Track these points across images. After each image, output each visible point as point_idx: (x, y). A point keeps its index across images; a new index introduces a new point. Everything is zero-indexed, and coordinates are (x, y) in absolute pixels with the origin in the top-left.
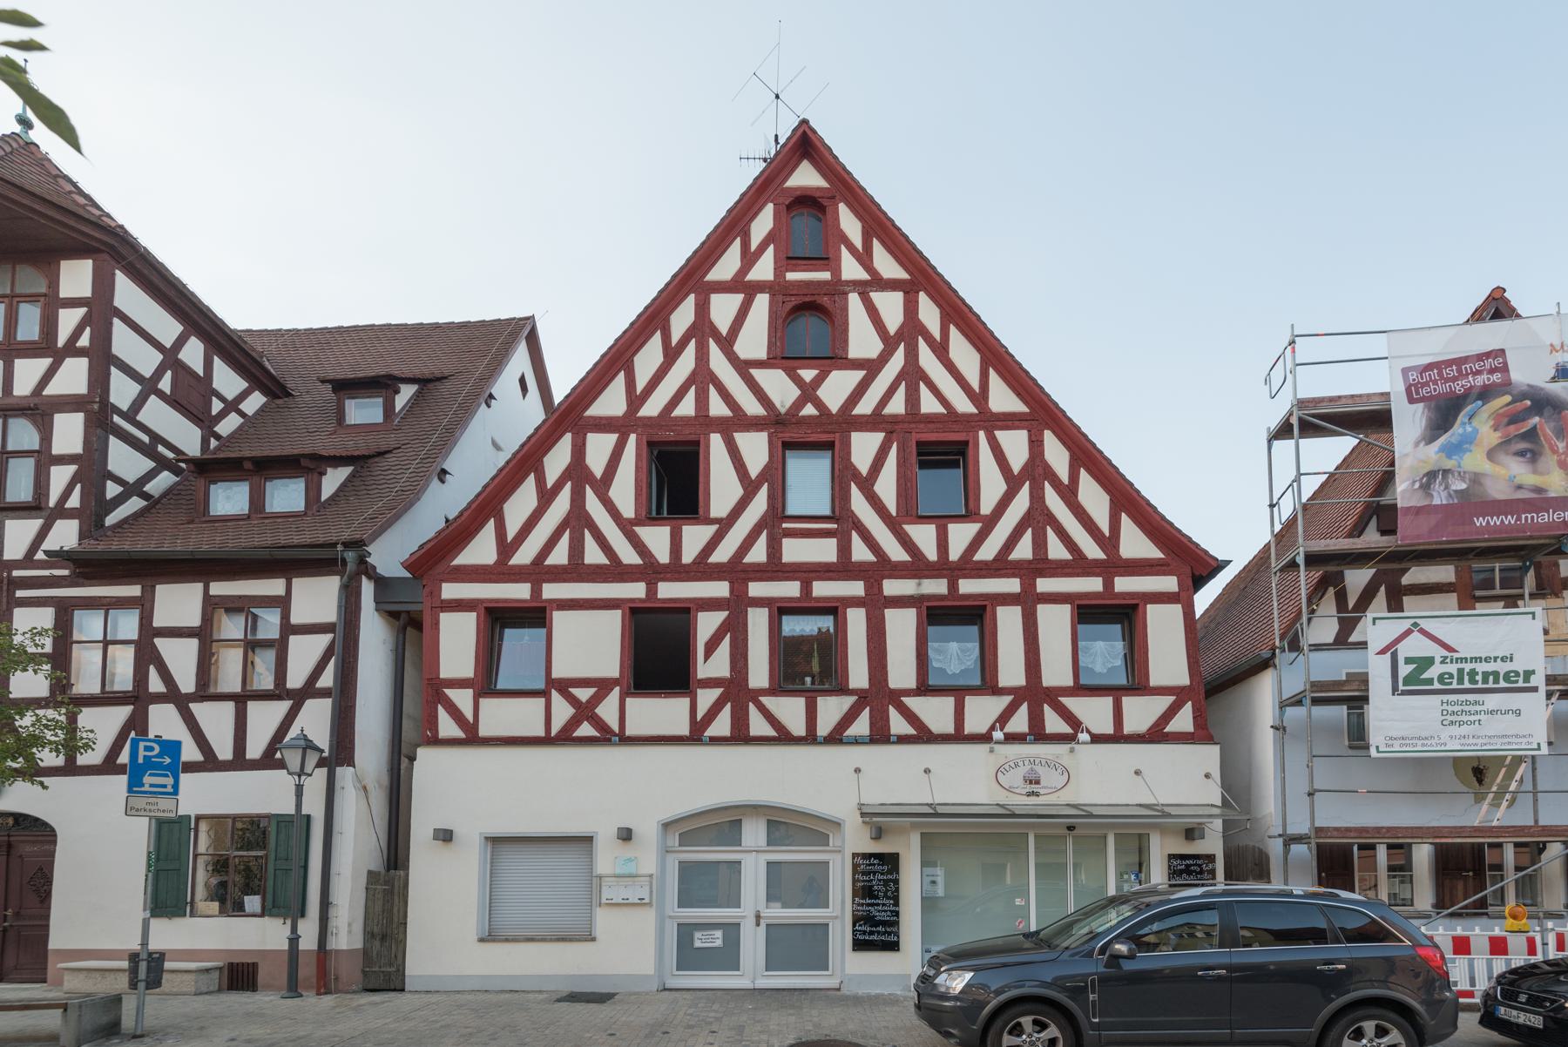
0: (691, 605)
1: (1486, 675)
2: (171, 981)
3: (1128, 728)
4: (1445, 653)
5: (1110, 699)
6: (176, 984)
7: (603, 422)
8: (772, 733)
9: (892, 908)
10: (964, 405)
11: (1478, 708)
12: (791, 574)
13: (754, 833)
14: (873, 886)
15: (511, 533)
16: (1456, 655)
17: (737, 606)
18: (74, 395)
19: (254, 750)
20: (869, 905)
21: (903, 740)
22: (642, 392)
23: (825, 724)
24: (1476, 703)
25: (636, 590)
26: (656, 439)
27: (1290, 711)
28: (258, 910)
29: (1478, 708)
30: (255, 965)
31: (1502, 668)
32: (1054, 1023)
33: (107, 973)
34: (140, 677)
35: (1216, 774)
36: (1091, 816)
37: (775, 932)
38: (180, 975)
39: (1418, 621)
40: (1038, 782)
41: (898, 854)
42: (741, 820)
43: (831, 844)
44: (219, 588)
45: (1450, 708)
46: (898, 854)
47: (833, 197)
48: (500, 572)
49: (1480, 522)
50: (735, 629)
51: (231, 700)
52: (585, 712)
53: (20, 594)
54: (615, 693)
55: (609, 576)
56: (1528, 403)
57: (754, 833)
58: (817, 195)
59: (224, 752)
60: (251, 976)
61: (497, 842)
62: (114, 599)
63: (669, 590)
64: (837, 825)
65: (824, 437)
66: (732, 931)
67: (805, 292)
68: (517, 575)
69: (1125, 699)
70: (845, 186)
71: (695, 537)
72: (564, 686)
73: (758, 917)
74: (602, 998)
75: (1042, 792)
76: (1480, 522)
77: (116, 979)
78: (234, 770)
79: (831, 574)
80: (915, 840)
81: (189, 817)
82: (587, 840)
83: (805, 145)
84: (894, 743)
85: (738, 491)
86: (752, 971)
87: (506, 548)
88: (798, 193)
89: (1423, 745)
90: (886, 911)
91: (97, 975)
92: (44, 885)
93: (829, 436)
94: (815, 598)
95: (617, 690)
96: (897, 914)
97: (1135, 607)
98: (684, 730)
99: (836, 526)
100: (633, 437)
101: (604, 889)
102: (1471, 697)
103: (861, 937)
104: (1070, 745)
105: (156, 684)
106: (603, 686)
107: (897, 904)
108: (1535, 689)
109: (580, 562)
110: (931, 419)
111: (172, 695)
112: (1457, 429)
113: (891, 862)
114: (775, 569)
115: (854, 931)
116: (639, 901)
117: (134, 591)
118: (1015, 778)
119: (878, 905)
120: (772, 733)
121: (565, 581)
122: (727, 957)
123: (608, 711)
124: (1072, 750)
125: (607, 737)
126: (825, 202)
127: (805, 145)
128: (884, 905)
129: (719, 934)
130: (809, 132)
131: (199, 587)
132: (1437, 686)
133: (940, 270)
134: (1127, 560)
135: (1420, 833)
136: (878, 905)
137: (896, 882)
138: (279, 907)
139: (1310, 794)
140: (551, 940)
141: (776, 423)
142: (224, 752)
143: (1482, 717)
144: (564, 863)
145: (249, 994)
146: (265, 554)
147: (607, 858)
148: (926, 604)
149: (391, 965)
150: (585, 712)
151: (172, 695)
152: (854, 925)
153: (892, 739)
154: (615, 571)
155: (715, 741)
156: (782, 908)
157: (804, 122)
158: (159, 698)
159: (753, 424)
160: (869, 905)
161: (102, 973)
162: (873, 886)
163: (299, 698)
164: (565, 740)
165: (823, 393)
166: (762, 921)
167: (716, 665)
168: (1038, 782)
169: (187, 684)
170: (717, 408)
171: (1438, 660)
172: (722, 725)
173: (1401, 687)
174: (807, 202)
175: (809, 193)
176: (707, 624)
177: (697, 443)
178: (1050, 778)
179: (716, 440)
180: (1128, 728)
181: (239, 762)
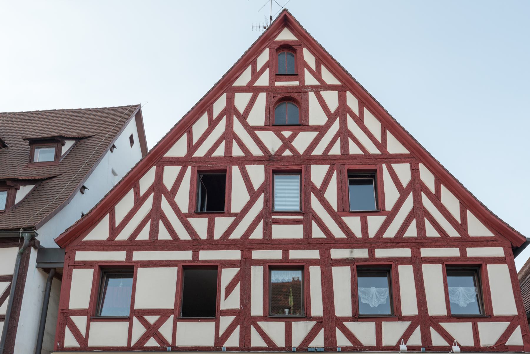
15: (118, 223)
26: (203, 169)
47: (300, 45)
84: (339, 352)
87: (114, 231)
88: (282, 43)
95: (172, 317)
97: (480, 266)
99: (302, 217)
106: (164, 314)
110: (356, 157)
126: (296, 47)
134: (473, 238)
148: (356, 264)
175: (288, 43)
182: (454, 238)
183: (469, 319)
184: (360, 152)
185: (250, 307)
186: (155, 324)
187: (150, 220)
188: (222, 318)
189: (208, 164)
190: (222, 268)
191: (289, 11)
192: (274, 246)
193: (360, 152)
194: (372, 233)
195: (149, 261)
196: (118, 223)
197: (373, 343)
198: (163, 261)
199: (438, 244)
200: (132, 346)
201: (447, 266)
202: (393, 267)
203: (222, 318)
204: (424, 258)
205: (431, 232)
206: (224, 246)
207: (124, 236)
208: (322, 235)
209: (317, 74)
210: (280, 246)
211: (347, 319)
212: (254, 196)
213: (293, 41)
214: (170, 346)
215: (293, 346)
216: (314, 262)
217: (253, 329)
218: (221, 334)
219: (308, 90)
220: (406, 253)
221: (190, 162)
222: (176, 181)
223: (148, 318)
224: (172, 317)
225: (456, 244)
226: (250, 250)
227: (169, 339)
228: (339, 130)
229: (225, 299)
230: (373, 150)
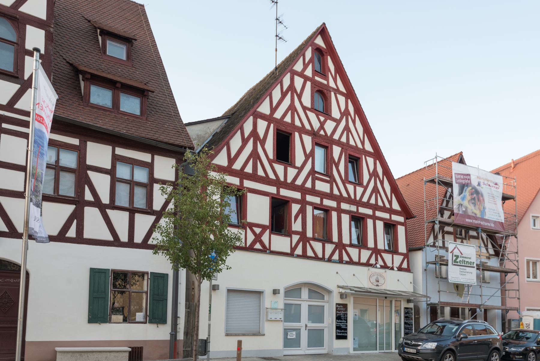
0: (290, 200)
1: (467, 262)
2: (117, 357)
3: (361, 261)
4: (461, 255)
5: (61, 193)
6: (119, 358)
7: (263, 115)
8: (313, 255)
9: (346, 324)
10: (360, 146)
11: (465, 271)
12: (317, 194)
13: (305, 293)
14: (341, 316)
15: (233, 155)
16: (463, 256)
17: (303, 202)
18: (38, 18)
19: (138, 238)
20: (340, 322)
21: (347, 263)
22: (275, 107)
23: (364, 260)
24: (465, 269)
25: (272, 190)
26: (279, 128)
27: (430, 265)
28: (142, 320)
29: (465, 271)
30: (141, 348)
31: (466, 260)
32: (453, 356)
33: (83, 354)
34: (80, 192)
35: (412, 282)
36: (370, 292)
37: (311, 332)
38: (121, 353)
39: (457, 245)
40: (378, 282)
41: (347, 304)
42: (301, 288)
43: (325, 299)
44: (120, 151)
45: (462, 270)
46: (347, 304)
47: (326, 53)
48: (228, 170)
49: (467, 220)
50: (302, 211)
51: (127, 211)
52: (258, 238)
53: (4, 126)
54: (268, 231)
55: (265, 181)
56: (474, 190)
57: (305, 293)
58: (323, 50)
59: (124, 237)
60: (132, 356)
61: (229, 291)
62: (63, 143)
63: (284, 192)
64: (329, 292)
65: (326, 144)
66: (298, 331)
67: (320, 86)
68: (234, 173)
69: (326, 244)
70: (331, 50)
71: (292, 172)
72: (251, 226)
73: (306, 326)
74: (279, 360)
75: (379, 285)
76: (467, 220)
77: (88, 357)
78: (129, 248)
79: (328, 197)
80: (352, 299)
81: (109, 269)
82: (259, 293)
83: (323, 31)
84: (344, 264)
85: (303, 158)
86: (304, 349)
87: (232, 161)
88: (318, 47)
89: (454, 279)
90: (344, 325)
91: (78, 355)
92: (8, 303)
93: (328, 144)
94: (324, 205)
95: (268, 231)
96: (347, 326)
97: (363, 218)
98: (289, 251)
99: (329, 179)
100: (272, 125)
101: (269, 314)
102: (464, 268)
103: (338, 334)
104: (385, 270)
105: (88, 196)
106: (264, 228)
107: (347, 322)
108: (474, 267)
109: (256, 173)
110: (352, 147)
111: (97, 203)
112: (463, 194)
113: (345, 306)
114: (313, 192)
115: (336, 332)
116: (280, 320)
117: (75, 142)
118: (373, 280)
119: (342, 322)
120: (313, 255)
121: (251, 180)
122: (296, 343)
123: (265, 238)
124: (385, 272)
125: (266, 250)
126: (324, 53)
127: (323, 31)
128: (344, 322)
129: (294, 333)
130: (325, 27)
131: (110, 148)
132: (459, 264)
133: (357, 96)
134: (394, 209)
135: (448, 304)
136: (342, 322)
137: (347, 314)
138: (155, 319)
139: (439, 292)
140: (251, 335)
141: (313, 134)
142: (124, 237)
143: (466, 273)
144: (250, 301)
145: (350, 349)
146: (153, 143)
147: (268, 301)
148: (352, 214)
149: (189, 347)
150: (258, 238)
151: (97, 203)
152: (336, 330)
153: (344, 262)
154: (266, 180)
155: (298, 256)
156: (312, 323)
157: (324, 24)
158: (90, 204)
159: (307, 133)
160: (340, 322)
161: (80, 353)
162: (341, 316)
163: (159, 215)
164: (251, 249)
165: (326, 126)
166: (307, 328)
167: (297, 226)
168: (378, 282)
169: (105, 199)
170: (297, 123)
171: (460, 256)
172: (299, 251)
173: (453, 263)
174: (318, 50)
175: (320, 48)
176: (295, 208)
177: (291, 134)
178: (381, 281)
179: (297, 134)
180: (361, 261)
181: (131, 244)
182: (388, 208)
183: (390, 253)
184: (354, 145)
185: (306, 231)
186: (259, 234)
187: (252, 159)
188: (293, 236)
189: (282, 126)
190: (292, 203)
191: (326, 25)
192: (316, 194)
193: (354, 145)
194: (289, 180)
195: (253, 189)
196: (233, 155)
197: (357, 260)
198: (261, 191)
199: (382, 210)
200: (247, 247)
201: (352, 216)
202: (365, 219)
203: (293, 236)
204: (377, 216)
205: (380, 203)
206: (292, 188)
207: (237, 166)
208: (338, 193)
209: (305, 66)
210: (320, 195)
211: (347, 246)
212: (307, 157)
213: (323, 48)
214: (268, 250)
215: (325, 258)
216: (296, 201)
217: (308, 244)
218: (293, 246)
219: (331, 90)
220: (297, 195)
221: (272, 120)
222: (265, 133)
223: (256, 229)
224: (268, 231)
225: (388, 211)
226: (306, 194)
227: (267, 244)
228: (290, 104)
229: (294, 223)
230: (360, 146)
